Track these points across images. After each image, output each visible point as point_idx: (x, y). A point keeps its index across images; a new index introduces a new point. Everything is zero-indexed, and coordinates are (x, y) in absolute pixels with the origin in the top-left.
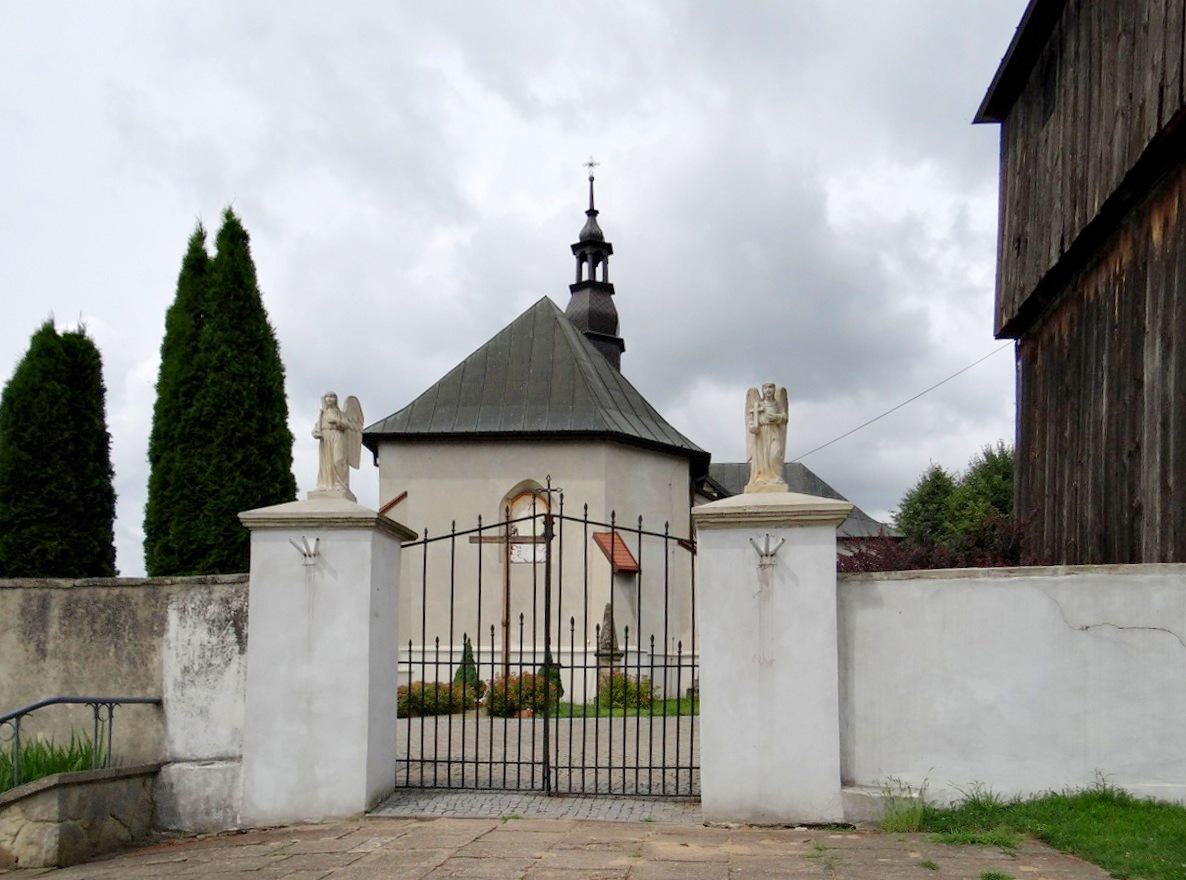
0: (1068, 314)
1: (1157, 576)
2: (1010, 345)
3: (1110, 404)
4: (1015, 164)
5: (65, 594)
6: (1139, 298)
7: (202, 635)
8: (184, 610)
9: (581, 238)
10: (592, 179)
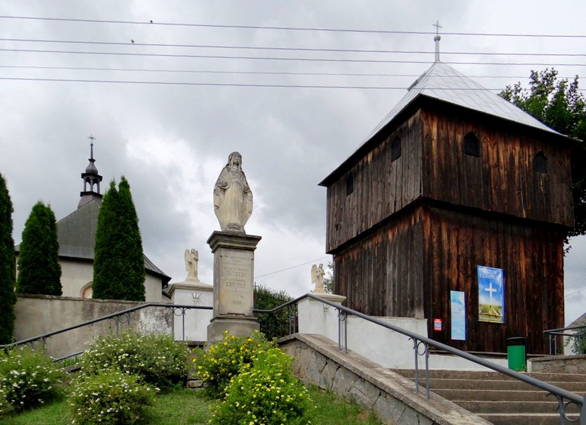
0: (356, 252)
1: (406, 320)
2: (331, 256)
3: (374, 278)
4: (334, 203)
5: (100, 304)
6: (385, 251)
7: (153, 321)
8: (146, 312)
9: (87, 171)
10: (92, 145)
